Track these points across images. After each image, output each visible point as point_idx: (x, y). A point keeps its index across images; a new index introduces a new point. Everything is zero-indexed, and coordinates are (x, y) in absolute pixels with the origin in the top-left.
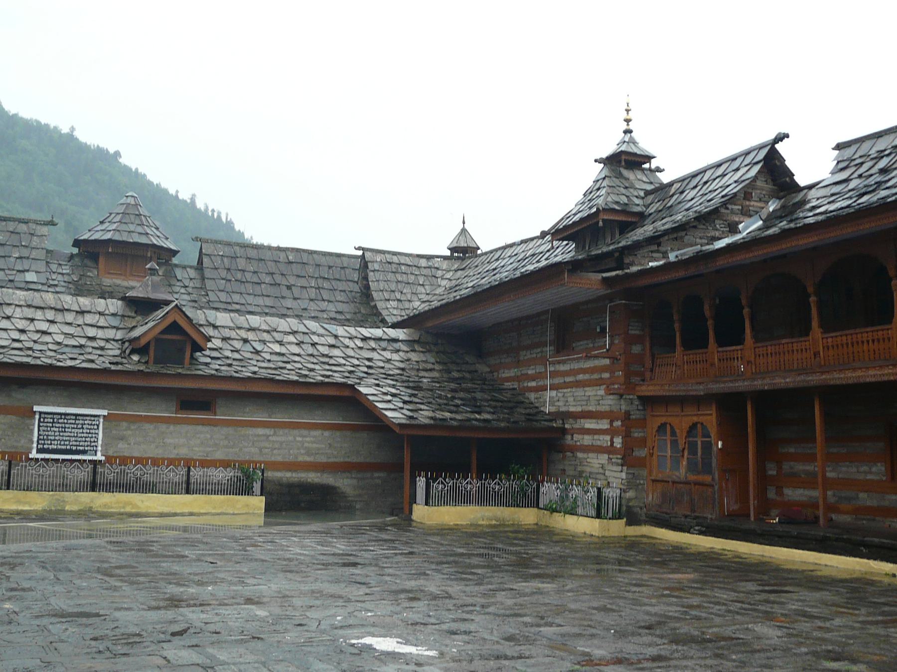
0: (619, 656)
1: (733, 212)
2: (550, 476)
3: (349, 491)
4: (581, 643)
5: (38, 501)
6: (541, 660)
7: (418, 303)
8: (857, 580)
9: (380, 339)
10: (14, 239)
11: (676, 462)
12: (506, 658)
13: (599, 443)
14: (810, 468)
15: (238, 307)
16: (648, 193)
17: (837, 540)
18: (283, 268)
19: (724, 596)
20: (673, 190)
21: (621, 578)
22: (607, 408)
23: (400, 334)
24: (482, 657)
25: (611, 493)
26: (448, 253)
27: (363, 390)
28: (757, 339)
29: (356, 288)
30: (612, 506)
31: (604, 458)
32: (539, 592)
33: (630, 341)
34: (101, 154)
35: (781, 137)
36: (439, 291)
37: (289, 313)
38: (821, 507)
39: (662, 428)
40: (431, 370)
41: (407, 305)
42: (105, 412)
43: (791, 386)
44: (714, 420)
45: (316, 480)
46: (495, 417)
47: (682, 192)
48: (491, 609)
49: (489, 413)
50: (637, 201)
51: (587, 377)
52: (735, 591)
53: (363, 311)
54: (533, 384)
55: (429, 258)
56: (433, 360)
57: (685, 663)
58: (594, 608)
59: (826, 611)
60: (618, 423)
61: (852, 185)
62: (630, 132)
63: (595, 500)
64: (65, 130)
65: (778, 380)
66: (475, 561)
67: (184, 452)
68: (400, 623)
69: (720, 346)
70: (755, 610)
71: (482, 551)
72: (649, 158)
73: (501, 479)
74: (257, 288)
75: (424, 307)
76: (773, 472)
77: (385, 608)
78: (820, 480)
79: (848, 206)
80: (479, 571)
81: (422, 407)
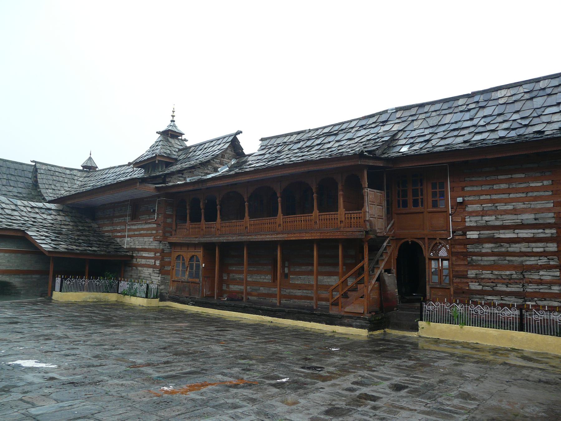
0: (149, 362)
1: (216, 163)
2: (125, 278)
3: (18, 285)
4: (132, 357)
6: (111, 366)
7: (64, 192)
8: (257, 324)
9: (41, 208)
11: (184, 272)
12: (93, 366)
13: (149, 263)
14: (241, 276)
16: (180, 150)
17: (250, 307)
19: (200, 333)
20: (191, 150)
21: (154, 326)
22: (154, 247)
23: (52, 206)
24: (81, 367)
25: (153, 287)
26: (81, 168)
27: (30, 233)
28: (222, 219)
30: (153, 292)
31: (151, 270)
32: (114, 333)
33: (166, 217)
35: (239, 132)
36: (75, 186)
38: (244, 294)
39: (178, 257)
40: (67, 225)
41: (57, 192)
43: (235, 241)
44: (202, 255)
46: (99, 249)
47: (195, 152)
48: (88, 343)
49: (96, 247)
50: (174, 153)
51: (145, 232)
52: (205, 331)
53: (33, 193)
54: (119, 234)
55: (71, 170)
56: (69, 220)
57: (178, 364)
58: (140, 340)
59: (242, 338)
60: (158, 254)
61: (266, 156)
62: (174, 121)
63: (145, 290)
65: (230, 238)
66: (83, 319)
68: (38, 352)
69: (206, 222)
70: (213, 339)
71: (87, 314)
72: (181, 134)
73: (100, 279)
75: (67, 194)
76: (225, 278)
77: (31, 344)
78: (245, 282)
79: (263, 165)
80: (85, 324)
81: (62, 243)
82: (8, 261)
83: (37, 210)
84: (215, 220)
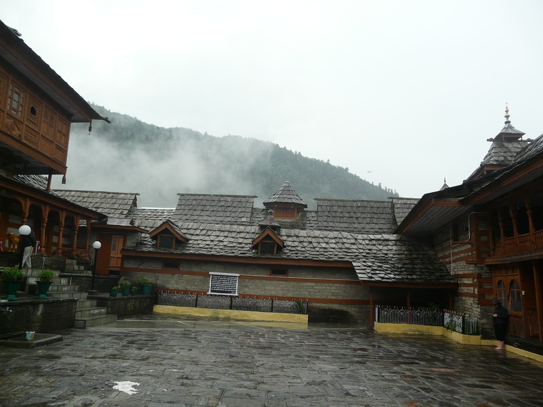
5: (207, 313)
9: (379, 240)
10: (240, 204)
15: (331, 228)
18: (354, 209)
22: (470, 272)
29: (391, 217)
34: (340, 169)
37: (355, 230)
42: (238, 275)
45: (337, 308)
62: (509, 122)
64: (326, 161)
67: (273, 293)
69: (520, 233)
72: (521, 135)
73: (421, 310)
74: (342, 219)
82: (344, 291)
83: (374, 242)
84: (529, 232)
